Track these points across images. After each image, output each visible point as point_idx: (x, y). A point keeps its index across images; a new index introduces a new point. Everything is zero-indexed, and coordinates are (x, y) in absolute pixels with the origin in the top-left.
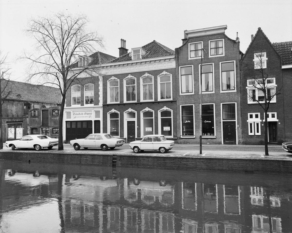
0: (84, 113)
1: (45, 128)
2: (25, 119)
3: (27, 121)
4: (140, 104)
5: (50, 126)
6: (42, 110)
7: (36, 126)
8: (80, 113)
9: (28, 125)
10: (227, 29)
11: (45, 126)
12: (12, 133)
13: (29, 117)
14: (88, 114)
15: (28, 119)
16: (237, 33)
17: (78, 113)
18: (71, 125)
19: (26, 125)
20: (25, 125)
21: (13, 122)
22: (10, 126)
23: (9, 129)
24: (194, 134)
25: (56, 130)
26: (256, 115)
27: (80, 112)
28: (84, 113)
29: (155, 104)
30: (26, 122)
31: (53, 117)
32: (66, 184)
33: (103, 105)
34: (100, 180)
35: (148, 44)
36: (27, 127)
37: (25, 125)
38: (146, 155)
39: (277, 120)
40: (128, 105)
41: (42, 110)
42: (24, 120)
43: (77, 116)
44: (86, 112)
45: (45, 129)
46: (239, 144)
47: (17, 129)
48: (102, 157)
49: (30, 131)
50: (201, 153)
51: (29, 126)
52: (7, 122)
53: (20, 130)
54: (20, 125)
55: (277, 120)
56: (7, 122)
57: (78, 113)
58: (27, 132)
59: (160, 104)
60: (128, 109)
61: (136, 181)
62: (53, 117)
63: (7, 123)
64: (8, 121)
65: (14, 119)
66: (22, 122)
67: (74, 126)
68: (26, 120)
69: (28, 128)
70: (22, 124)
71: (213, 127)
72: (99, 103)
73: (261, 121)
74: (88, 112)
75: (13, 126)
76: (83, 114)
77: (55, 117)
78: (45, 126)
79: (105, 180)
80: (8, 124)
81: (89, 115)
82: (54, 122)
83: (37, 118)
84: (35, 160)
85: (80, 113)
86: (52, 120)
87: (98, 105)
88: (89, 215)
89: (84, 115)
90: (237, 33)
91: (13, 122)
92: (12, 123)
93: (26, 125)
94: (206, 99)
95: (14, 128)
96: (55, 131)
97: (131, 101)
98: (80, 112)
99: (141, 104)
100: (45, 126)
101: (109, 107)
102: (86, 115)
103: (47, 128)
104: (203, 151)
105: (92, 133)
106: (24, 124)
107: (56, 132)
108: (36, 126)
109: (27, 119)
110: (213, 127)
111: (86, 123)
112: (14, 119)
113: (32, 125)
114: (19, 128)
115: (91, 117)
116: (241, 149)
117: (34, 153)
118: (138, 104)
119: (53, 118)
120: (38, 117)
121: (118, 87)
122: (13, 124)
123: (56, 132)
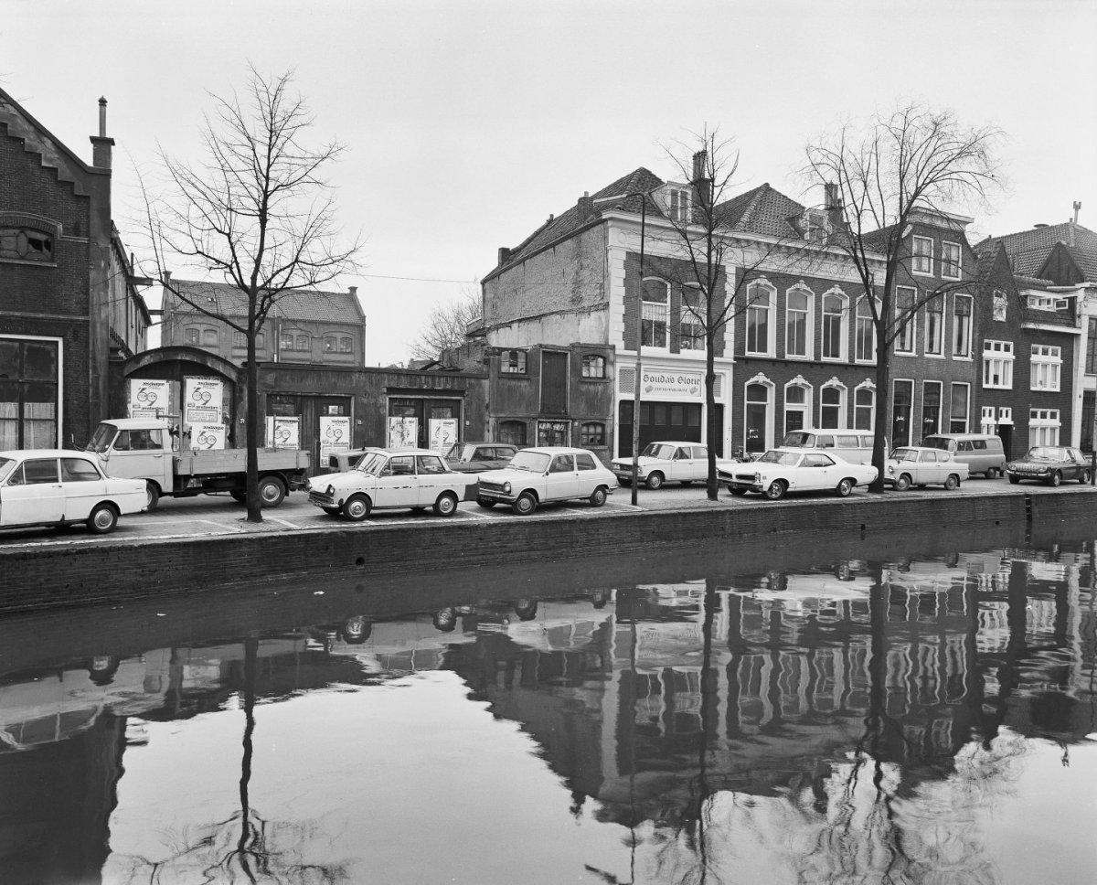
0: (676, 377)
1: (546, 422)
2: (473, 381)
3: (483, 393)
6: (543, 352)
7: (520, 414)
8: (666, 375)
9: (487, 407)
10: (767, 184)
11: (556, 416)
12: (407, 440)
13: (491, 376)
14: (689, 381)
16: (103, 102)
17: (657, 375)
21: (421, 391)
22: (398, 409)
23: (395, 420)
25: (592, 430)
27: (664, 374)
28: (676, 377)
29: (849, 368)
30: (480, 397)
31: (586, 383)
34: (835, 580)
35: (1020, 234)
39: (1012, 423)
40: (837, 367)
41: (543, 352)
42: (470, 384)
43: (655, 385)
44: (684, 376)
45: (548, 426)
47: (434, 423)
49: (493, 432)
51: (495, 411)
52: (391, 390)
53: (444, 430)
55: (1012, 423)
56: (391, 390)
57: (657, 375)
59: (825, 368)
62: (586, 383)
64: (393, 384)
65: (423, 378)
66: (461, 393)
68: (481, 386)
70: (459, 401)
71: (360, 422)
75: (412, 411)
76: (672, 380)
78: (556, 416)
79: (844, 580)
80: (390, 399)
82: (587, 402)
83: (524, 384)
84: (492, 548)
85: (666, 375)
86: (582, 393)
87: (722, 356)
88: (691, 703)
89: (676, 385)
90: (103, 102)
91: (421, 391)
92: (413, 397)
94: (933, 370)
96: (588, 434)
97: (863, 360)
98: (664, 374)
100: (552, 416)
101: (750, 367)
102: (683, 386)
105: (907, 445)
106: (469, 404)
107: (592, 440)
109: (484, 381)
110: (360, 422)
111: (681, 412)
112: (423, 378)
113: (502, 411)
119: (584, 388)
120: (528, 379)
121: (790, 307)
122: (412, 399)
123: (591, 437)
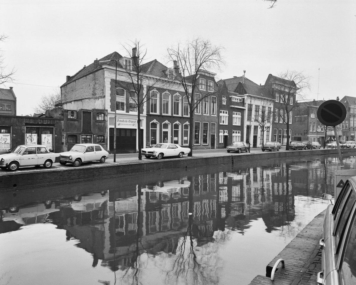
3: (61, 125)
4: (173, 117)
5: (94, 133)
7: (75, 132)
9: (63, 130)
12: (33, 142)
13: (65, 119)
15: (62, 122)
17: (122, 120)
18: (120, 133)
19: (60, 130)
20: (58, 130)
21: (38, 124)
22: (30, 131)
23: (28, 135)
24: (200, 143)
25: (100, 138)
26: (238, 132)
28: (128, 120)
29: (182, 118)
30: (61, 126)
32: (182, 188)
33: (147, 115)
36: (61, 133)
37: (58, 130)
38: (98, 165)
39: (228, 135)
42: (57, 122)
43: (121, 123)
45: (85, 136)
46: (216, 148)
47: (43, 136)
48: (130, 166)
49: (65, 139)
50: (115, 161)
51: (65, 132)
52: (26, 124)
54: (47, 130)
55: (228, 135)
56: (26, 124)
57: (122, 120)
58: (61, 140)
60: (186, 122)
61: (77, 198)
63: (25, 125)
64: (28, 122)
65: (39, 120)
66: (53, 125)
67: (123, 134)
68: (61, 123)
69: (63, 134)
72: (143, 112)
73: (223, 135)
74: (132, 120)
76: (127, 122)
77: (99, 122)
80: (26, 127)
81: (133, 123)
83: (76, 122)
85: (125, 120)
87: (143, 114)
88: (133, 227)
89: (128, 123)
91: (38, 124)
93: (60, 130)
95: (36, 134)
99: (159, 117)
101: (152, 117)
102: (130, 123)
103: (83, 135)
104: (117, 160)
106: (56, 129)
108: (75, 133)
109: (62, 121)
113: (69, 131)
114: (47, 135)
115: (135, 125)
116: (218, 151)
117: (202, 159)
118: (172, 118)
120: (78, 121)
123: (100, 140)
